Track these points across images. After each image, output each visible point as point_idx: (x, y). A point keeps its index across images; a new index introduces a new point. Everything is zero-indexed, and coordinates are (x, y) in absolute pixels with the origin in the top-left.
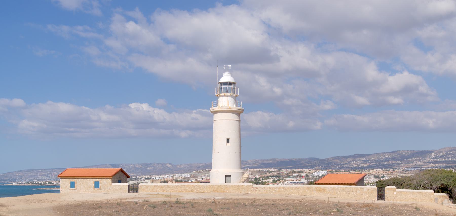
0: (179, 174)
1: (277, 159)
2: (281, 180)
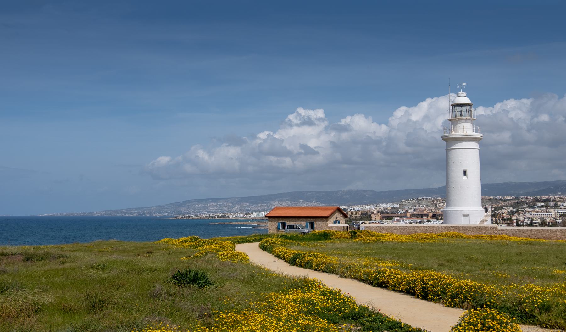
0: (384, 204)
2: (520, 210)
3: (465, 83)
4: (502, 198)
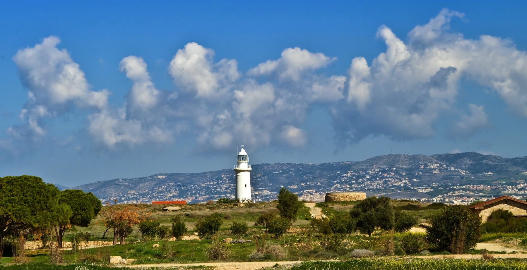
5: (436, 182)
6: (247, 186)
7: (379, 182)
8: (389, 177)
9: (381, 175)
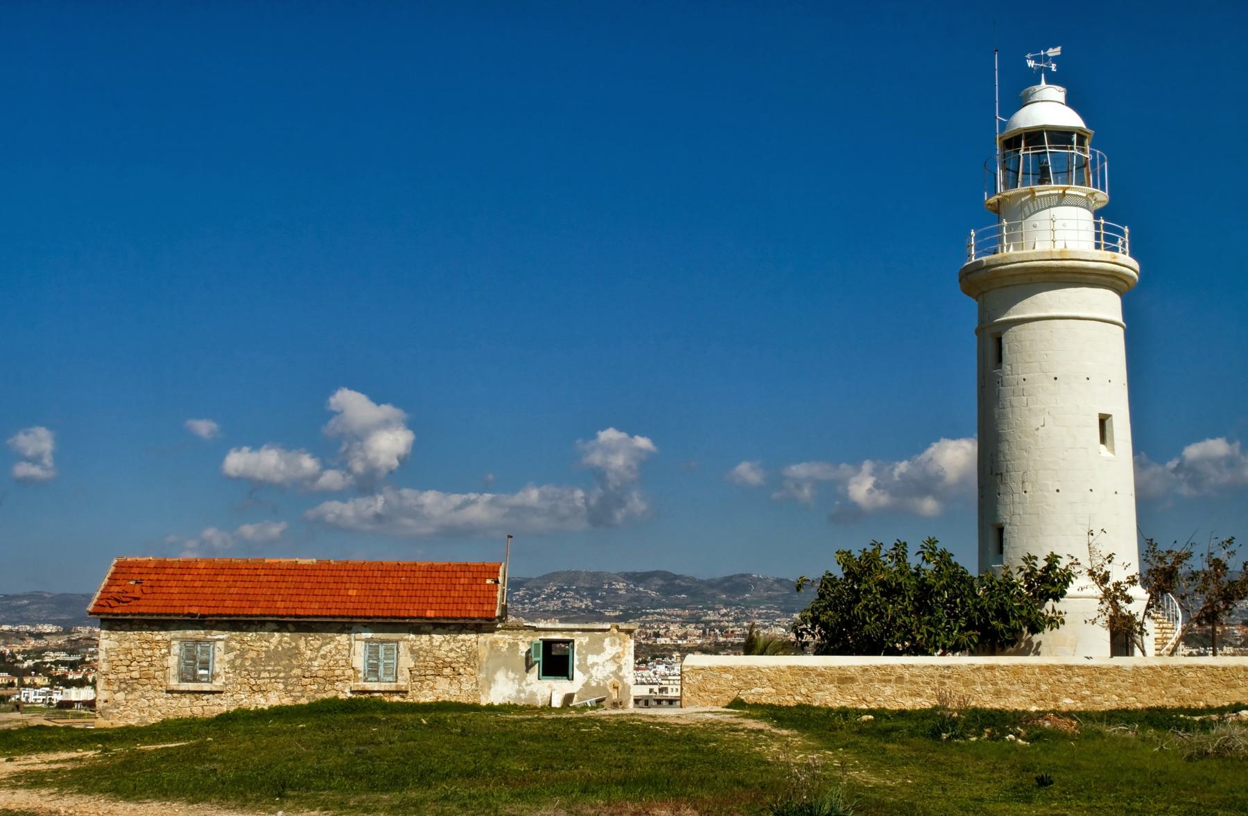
1: (46, 595)
3: (1059, 49)
4: (32, 630)
5: (622, 605)
6: (1118, 492)
7: (556, 603)
8: (568, 597)
9: (558, 594)
